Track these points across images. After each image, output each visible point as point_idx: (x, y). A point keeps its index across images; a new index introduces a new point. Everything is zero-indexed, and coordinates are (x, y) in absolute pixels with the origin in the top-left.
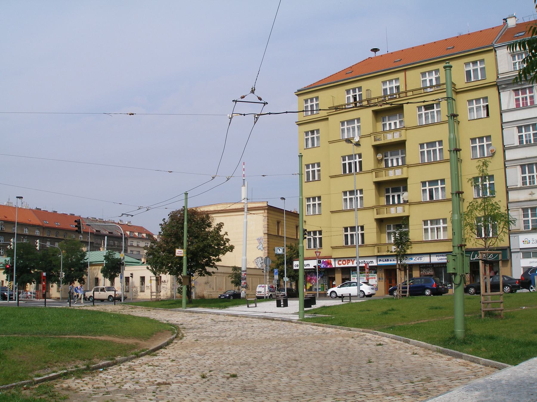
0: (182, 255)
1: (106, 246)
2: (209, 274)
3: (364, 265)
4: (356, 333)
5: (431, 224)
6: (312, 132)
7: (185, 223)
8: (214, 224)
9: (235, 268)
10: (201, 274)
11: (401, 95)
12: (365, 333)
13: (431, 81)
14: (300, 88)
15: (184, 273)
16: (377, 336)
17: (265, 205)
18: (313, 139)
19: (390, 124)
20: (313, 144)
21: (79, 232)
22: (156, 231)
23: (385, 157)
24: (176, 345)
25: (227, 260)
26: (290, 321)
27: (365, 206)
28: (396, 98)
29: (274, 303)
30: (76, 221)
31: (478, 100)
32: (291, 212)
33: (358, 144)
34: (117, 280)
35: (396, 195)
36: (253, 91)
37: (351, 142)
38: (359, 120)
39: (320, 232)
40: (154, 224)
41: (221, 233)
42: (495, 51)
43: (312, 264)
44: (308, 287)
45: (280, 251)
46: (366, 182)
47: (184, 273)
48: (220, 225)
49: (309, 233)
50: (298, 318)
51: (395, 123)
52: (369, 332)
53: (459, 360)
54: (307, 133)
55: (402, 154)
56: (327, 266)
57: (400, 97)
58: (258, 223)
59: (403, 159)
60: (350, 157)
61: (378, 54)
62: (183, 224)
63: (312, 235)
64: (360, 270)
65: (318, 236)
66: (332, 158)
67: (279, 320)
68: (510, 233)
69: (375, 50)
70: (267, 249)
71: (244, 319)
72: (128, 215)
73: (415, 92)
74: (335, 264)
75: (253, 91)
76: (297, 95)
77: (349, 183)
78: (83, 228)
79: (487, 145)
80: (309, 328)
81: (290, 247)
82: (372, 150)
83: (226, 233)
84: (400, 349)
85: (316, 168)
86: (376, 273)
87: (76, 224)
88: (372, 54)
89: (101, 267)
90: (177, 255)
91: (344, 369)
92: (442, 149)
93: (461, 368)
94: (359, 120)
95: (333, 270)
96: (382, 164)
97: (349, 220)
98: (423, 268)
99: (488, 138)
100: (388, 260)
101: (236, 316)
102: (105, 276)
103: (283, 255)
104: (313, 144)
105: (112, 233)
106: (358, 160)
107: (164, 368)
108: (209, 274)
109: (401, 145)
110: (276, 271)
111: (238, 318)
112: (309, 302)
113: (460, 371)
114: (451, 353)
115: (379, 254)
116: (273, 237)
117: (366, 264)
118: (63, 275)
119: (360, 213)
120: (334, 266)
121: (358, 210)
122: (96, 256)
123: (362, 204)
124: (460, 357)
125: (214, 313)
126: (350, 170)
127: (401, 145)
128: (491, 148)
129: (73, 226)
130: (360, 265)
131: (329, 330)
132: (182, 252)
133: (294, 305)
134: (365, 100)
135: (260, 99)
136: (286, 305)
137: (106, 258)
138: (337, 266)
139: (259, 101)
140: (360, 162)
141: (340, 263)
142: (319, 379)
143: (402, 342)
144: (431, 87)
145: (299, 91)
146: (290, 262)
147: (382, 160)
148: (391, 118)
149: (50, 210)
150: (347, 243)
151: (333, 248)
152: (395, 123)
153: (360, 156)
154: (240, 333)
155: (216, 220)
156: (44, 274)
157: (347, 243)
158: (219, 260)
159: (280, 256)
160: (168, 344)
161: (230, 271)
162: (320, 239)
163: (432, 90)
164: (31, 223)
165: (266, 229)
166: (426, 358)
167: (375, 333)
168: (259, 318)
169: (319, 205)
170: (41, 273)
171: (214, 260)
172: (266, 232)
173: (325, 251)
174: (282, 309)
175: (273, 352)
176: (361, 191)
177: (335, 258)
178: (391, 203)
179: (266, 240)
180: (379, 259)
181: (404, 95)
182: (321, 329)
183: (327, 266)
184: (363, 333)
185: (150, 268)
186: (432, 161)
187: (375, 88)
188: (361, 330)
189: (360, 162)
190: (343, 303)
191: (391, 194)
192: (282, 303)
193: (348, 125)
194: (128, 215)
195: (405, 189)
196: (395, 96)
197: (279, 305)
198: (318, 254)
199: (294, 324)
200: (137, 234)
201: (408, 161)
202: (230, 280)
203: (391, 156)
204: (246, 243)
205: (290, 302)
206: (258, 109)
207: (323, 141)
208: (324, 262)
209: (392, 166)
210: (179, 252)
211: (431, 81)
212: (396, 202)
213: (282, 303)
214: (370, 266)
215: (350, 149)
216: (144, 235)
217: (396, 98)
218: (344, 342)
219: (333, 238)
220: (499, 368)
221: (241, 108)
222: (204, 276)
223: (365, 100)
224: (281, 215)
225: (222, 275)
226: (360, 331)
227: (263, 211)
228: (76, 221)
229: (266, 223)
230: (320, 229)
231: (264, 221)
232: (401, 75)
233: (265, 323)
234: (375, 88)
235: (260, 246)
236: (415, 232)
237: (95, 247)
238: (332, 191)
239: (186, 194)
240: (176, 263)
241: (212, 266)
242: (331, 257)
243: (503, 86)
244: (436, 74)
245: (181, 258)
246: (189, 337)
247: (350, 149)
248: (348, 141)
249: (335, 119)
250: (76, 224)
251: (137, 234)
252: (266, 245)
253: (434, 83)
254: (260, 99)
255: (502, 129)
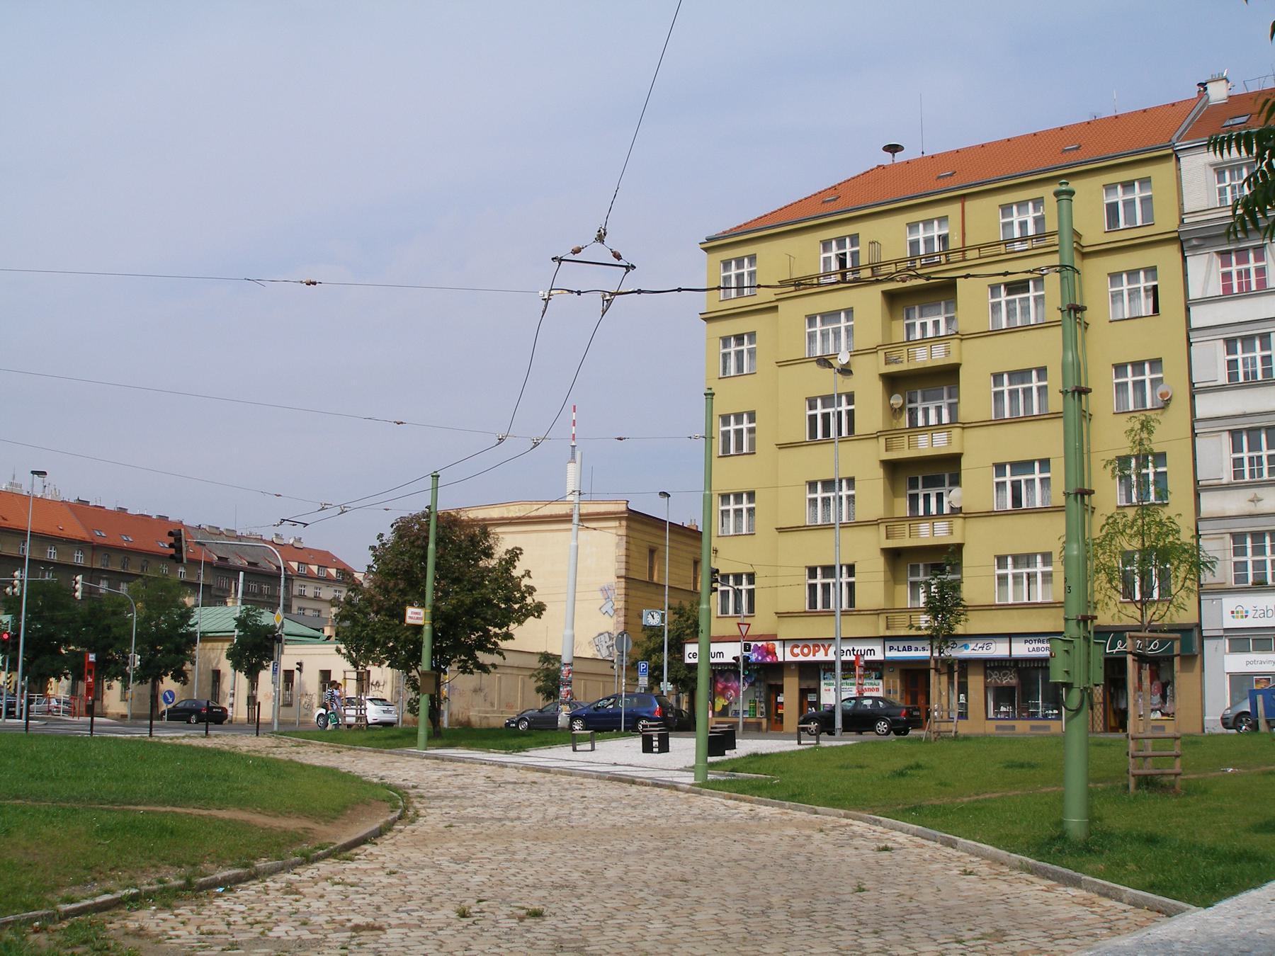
0: (420, 622)
1: (240, 595)
2: (483, 668)
3: (853, 658)
4: (829, 818)
5: (1015, 565)
6: (739, 339)
7: (431, 546)
8: (500, 551)
9: (546, 657)
10: (464, 669)
11: (952, 257)
12: (850, 821)
13: (1023, 225)
14: (712, 234)
15: (425, 665)
16: (879, 829)
17: (623, 508)
18: (739, 355)
19: (924, 326)
20: (740, 368)
21: (176, 558)
22: (360, 563)
23: (910, 402)
24: (400, 836)
25: (528, 637)
26: (673, 787)
27: (859, 517)
28: (939, 263)
29: (637, 742)
30: (171, 534)
31: (1133, 274)
32: (682, 527)
33: (846, 371)
34: (265, 676)
35: (933, 492)
36: (600, 238)
37: (831, 366)
38: (849, 312)
39: (751, 578)
40: (356, 546)
41: (516, 573)
42: (1178, 159)
43: (729, 652)
44: (718, 708)
45: (653, 619)
46: (863, 462)
47: (425, 665)
48: (514, 554)
49: (725, 577)
50: (692, 780)
51: (936, 323)
52: (860, 819)
53: (1073, 891)
54: (725, 341)
55: (950, 397)
56: (764, 657)
57: (948, 262)
58: (604, 552)
59: (953, 409)
60: (828, 400)
61: (900, 157)
62: (425, 548)
63: (731, 583)
64: (843, 670)
65: (745, 586)
66: (783, 400)
67: (647, 785)
68: (1202, 590)
69: (893, 149)
70: (622, 613)
71: (564, 779)
72: (295, 523)
73: (985, 252)
74: (783, 654)
75: (600, 238)
76: (706, 250)
77: (821, 461)
78: (188, 552)
79: (1152, 381)
80: (717, 803)
81: (679, 611)
82: (879, 386)
83: (528, 574)
84: (933, 860)
85: (745, 425)
86: (880, 678)
87: (172, 540)
88: (887, 158)
89: (227, 645)
90: (408, 621)
91: (798, 905)
92: (1046, 387)
93: (1077, 911)
94: (849, 312)
95: (779, 669)
96: (901, 418)
97: (821, 549)
98: (993, 669)
99: (1156, 363)
100: (910, 649)
101: (546, 770)
102: (237, 666)
103: (661, 629)
104: (740, 368)
105: (255, 564)
106: (844, 407)
107: (369, 890)
108: (483, 668)
109: (947, 376)
110: (643, 665)
111: (548, 777)
112: (720, 742)
113: (1074, 918)
114: (1055, 872)
115: (888, 633)
116: (638, 586)
117: (857, 656)
118: (136, 660)
119: (847, 534)
120: (780, 659)
121: (843, 526)
122: (217, 619)
123: (851, 513)
124: (1076, 883)
125: (493, 763)
126: (826, 432)
127: (947, 376)
128: (1161, 389)
129: (164, 545)
130: (844, 658)
131: (765, 811)
132: (422, 615)
133: (684, 749)
134: (865, 267)
135: (618, 257)
136: (664, 748)
137: (241, 623)
138: (789, 658)
139: (615, 261)
140: (851, 414)
141: (797, 651)
142: (738, 928)
143: (938, 845)
144: (1023, 239)
145: (709, 240)
146: (677, 647)
147: (901, 409)
148: (926, 311)
149: (111, 506)
150: (813, 603)
151: (780, 615)
152: (936, 323)
153: (851, 399)
154: (552, 811)
155: (505, 541)
156: (92, 657)
157: (813, 603)
158: (508, 636)
159: (655, 632)
160: (380, 833)
161: (535, 663)
162: (751, 593)
163: (1025, 246)
164: (65, 534)
165: (623, 565)
166: (994, 883)
167: (876, 820)
168: (600, 776)
169: (751, 511)
170: (83, 656)
171: (496, 635)
172: (623, 573)
173: (761, 623)
174: (655, 758)
175: (630, 860)
176: (851, 482)
177: (784, 641)
178: (921, 513)
179: (623, 591)
180: (888, 644)
181: (958, 256)
182: (745, 807)
183: (764, 657)
184: (845, 821)
185: (344, 651)
186: (1022, 414)
187: (890, 239)
188: (842, 812)
189: (851, 414)
190: (801, 747)
191: (921, 492)
192: (655, 744)
193: (823, 323)
194: (295, 523)
195: (956, 481)
196: (937, 259)
197: (647, 748)
198: (744, 628)
199: (682, 795)
200: (315, 568)
201: (965, 414)
202: (533, 684)
203: (924, 400)
204: (574, 601)
205: (674, 742)
206: (610, 279)
207: (765, 362)
208: (757, 648)
209: (927, 424)
210: (415, 615)
211: (1023, 225)
212: (933, 510)
213: (655, 744)
214: (866, 662)
215: (827, 381)
216: (333, 572)
217: (939, 263)
218: (801, 840)
219: (782, 591)
220: (1169, 913)
221: (572, 276)
222: (471, 673)
223: (865, 267)
224: (659, 532)
225: (515, 672)
226: (839, 816)
227: (616, 524)
228: (171, 534)
229: (623, 552)
230: (751, 570)
231: (618, 545)
232: (953, 210)
233: (613, 790)
234: (890, 239)
235: (608, 607)
236: (976, 582)
237: (215, 597)
238: (782, 479)
239: (436, 477)
240: (407, 641)
241: (491, 651)
242: (774, 638)
243: (1194, 242)
244: (1035, 209)
245: (418, 629)
246: (432, 819)
247: (827, 381)
248: (824, 362)
249: (794, 310)
250: (172, 540)
251: (315, 568)
252: (621, 604)
253: (1031, 231)
254: (618, 257)
255: (1190, 344)
